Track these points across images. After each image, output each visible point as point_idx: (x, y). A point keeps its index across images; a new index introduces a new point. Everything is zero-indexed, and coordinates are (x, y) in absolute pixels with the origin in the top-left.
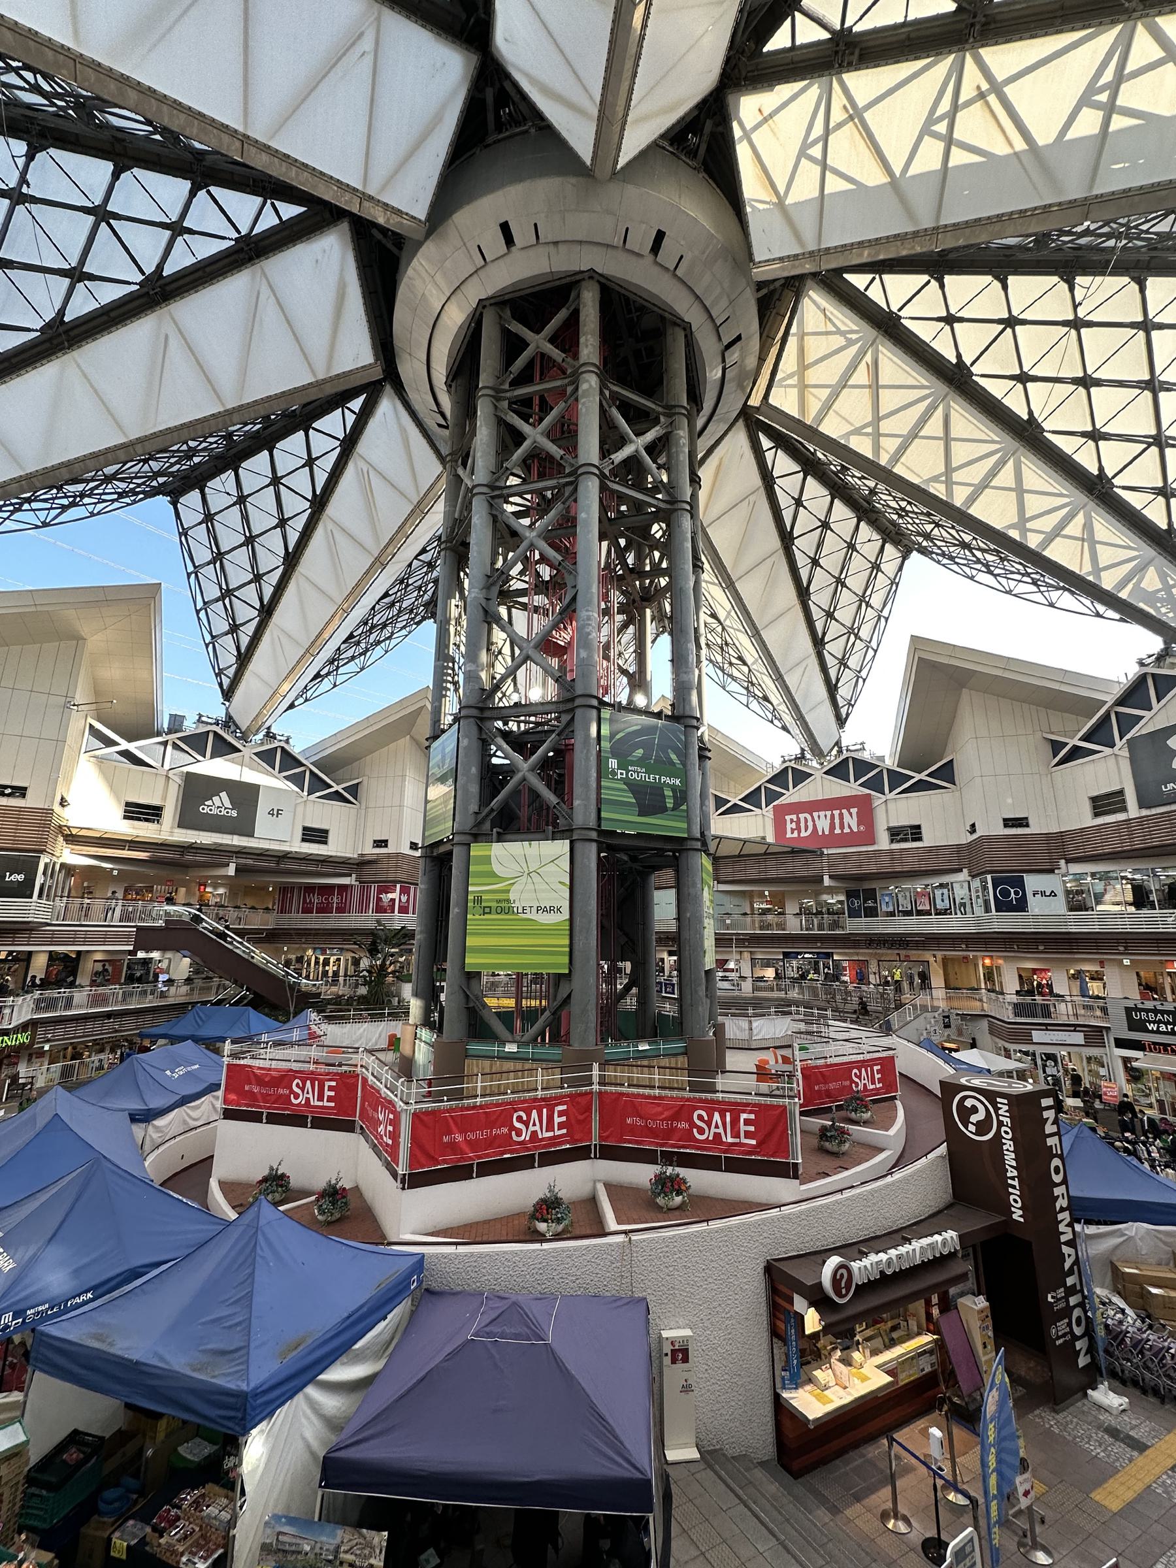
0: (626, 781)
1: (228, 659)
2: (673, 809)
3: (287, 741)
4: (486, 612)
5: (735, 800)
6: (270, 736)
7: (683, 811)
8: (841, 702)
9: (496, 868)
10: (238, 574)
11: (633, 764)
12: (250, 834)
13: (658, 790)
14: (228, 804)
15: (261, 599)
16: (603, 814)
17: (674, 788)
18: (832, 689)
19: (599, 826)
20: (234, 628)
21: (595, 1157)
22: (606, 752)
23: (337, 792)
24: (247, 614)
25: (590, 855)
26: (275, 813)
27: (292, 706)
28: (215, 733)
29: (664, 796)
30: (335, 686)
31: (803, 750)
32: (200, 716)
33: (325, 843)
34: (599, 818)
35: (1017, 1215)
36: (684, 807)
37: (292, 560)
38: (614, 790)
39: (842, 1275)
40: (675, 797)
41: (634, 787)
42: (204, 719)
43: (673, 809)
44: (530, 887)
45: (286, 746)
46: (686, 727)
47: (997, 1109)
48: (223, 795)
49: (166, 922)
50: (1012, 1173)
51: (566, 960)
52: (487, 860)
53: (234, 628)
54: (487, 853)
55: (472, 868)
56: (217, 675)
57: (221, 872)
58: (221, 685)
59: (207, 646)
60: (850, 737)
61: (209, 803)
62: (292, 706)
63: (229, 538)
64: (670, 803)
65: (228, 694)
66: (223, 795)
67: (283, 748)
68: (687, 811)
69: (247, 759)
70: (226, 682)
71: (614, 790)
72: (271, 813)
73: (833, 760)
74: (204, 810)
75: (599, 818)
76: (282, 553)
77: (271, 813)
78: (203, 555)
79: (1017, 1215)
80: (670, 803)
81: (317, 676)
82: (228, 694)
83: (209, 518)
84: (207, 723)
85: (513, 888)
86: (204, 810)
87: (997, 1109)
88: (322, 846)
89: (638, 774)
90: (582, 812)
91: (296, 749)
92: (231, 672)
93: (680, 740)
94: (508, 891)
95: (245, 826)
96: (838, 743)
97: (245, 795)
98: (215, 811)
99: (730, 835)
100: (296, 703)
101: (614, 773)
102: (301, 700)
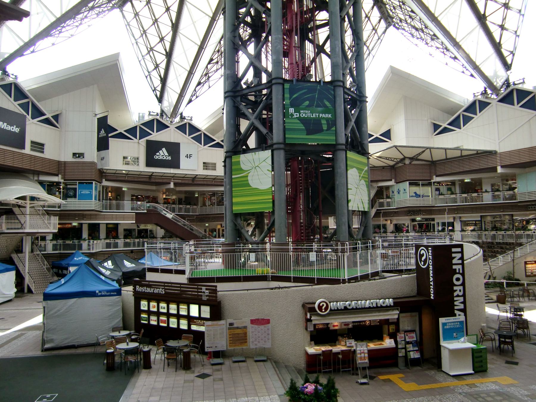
0: (299, 119)
1: (157, 83)
2: (327, 130)
3: (191, 120)
4: (234, 44)
5: (445, 125)
6: (182, 118)
7: (333, 130)
8: (505, 53)
9: (243, 166)
10: (154, 40)
11: (303, 109)
12: (177, 166)
13: (318, 121)
14: (166, 154)
15: (166, 50)
16: (287, 136)
17: (327, 120)
18: (497, 47)
19: (285, 142)
20: (157, 66)
21: (269, 280)
22: (287, 105)
23: (218, 143)
24: (161, 59)
25: (281, 156)
26: (189, 156)
27: (190, 101)
28: (157, 120)
29: (321, 124)
30: (210, 87)
31: (485, 88)
32: (150, 112)
33: (215, 170)
34: (285, 138)
35: (432, 298)
36: (334, 129)
37: (175, 27)
38: (293, 123)
39: (323, 305)
40: (328, 124)
41: (303, 121)
42: (152, 113)
43: (327, 130)
44: (256, 173)
45: (190, 122)
46: (335, 87)
47: (428, 252)
48: (164, 149)
49: (147, 210)
50: (431, 279)
51: (271, 205)
52: (238, 163)
53: (157, 66)
54: (238, 160)
55: (233, 167)
56: (153, 91)
57: (168, 187)
58: (156, 96)
59: (146, 77)
60: (514, 77)
61: (158, 154)
62: (190, 101)
63: (147, 22)
64: (325, 127)
65: (160, 100)
66: (164, 149)
67: (189, 123)
68: (336, 130)
69: (172, 130)
70: (158, 94)
71: (293, 123)
72: (187, 156)
73: (503, 92)
74: (156, 157)
75: (285, 138)
76: (170, 24)
77: (187, 156)
78: (137, 34)
79: (432, 298)
80: (325, 127)
81: (199, 84)
82: (160, 100)
83: (137, 14)
84: (153, 115)
85: (249, 174)
86: (156, 157)
87: (428, 252)
88: (214, 171)
89: (305, 114)
90: (277, 136)
91: (196, 123)
92: (159, 88)
93: (331, 94)
94: (247, 176)
95: (175, 163)
96: (507, 80)
97: (174, 149)
98: (161, 158)
99: (436, 146)
100: (193, 99)
101: (292, 115)
102: (195, 97)
